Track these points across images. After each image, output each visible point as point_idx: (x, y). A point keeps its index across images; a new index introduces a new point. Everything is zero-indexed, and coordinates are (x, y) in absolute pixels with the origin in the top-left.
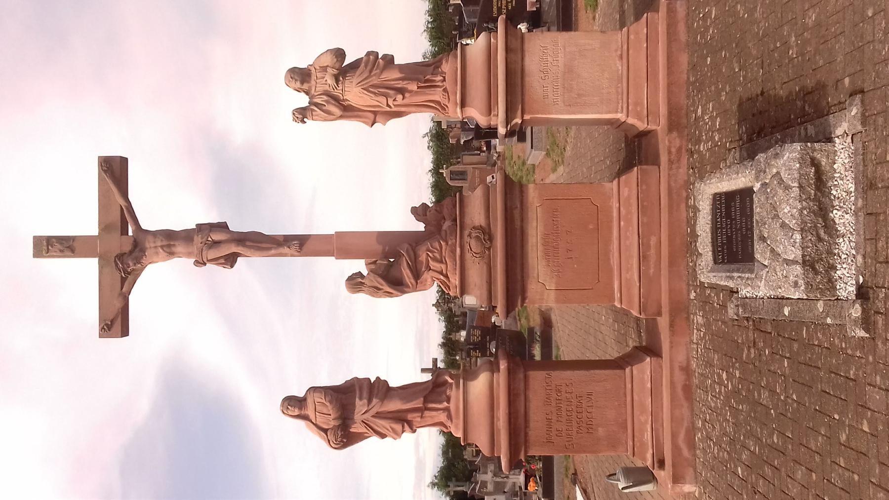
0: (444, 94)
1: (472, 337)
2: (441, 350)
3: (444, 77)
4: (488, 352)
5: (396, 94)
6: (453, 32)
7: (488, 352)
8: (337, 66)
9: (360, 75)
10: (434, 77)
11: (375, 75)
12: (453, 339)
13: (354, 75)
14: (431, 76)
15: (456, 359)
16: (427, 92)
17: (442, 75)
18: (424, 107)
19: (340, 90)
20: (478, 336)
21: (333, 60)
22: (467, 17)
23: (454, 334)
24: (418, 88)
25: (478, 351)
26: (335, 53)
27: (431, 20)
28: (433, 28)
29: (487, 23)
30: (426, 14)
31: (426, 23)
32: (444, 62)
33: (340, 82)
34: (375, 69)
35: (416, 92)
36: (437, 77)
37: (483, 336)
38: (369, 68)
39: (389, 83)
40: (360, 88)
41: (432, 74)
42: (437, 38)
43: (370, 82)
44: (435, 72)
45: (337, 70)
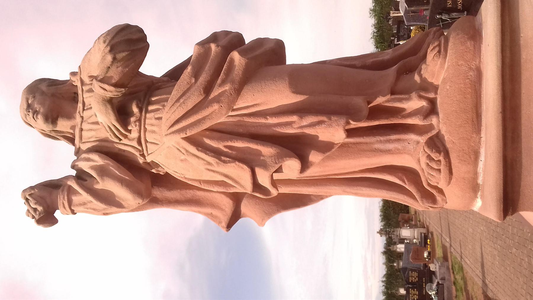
0: (433, 155)
1: (410, 278)
2: (383, 256)
3: (432, 102)
4: (424, 291)
5: (280, 157)
6: (391, 38)
7: (424, 291)
8: (115, 74)
9: (178, 100)
10: (400, 100)
11: (217, 100)
12: (392, 250)
13: (166, 100)
14: (389, 97)
15: (394, 266)
16: (377, 146)
17: (423, 94)
18: (369, 186)
19: (133, 139)
20: (415, 277)
21: (104, 58)
22: (407, 21)
23: (392, 246)
24: (350, 133)
25: (415, 289)
26: (110, 42)
27: (376, 31)
28: (377, 36)
29: (440, 14)
30: (372, 26)
31: (373, 33)
32: (430, 56)
33: (133, 119)
34: (219, 81)
35: (343, 146)
36: (409, 99)
37: (420, 277)
38: (203, 78)
39: (262, 121)
40: (178, 138)
41: (392, 93)
42: (380, 43)
43: (204, 119)
44: (403, 83)
45: (116, 85)
